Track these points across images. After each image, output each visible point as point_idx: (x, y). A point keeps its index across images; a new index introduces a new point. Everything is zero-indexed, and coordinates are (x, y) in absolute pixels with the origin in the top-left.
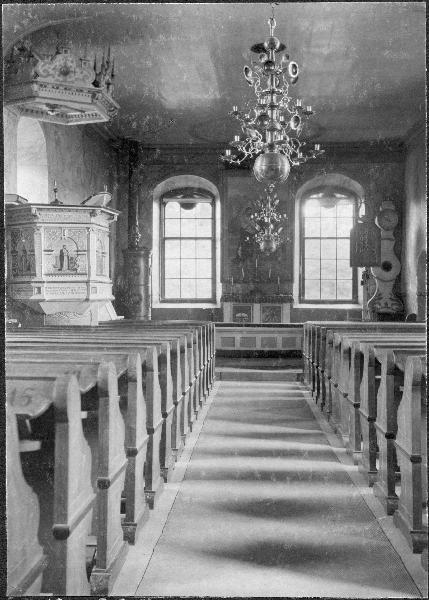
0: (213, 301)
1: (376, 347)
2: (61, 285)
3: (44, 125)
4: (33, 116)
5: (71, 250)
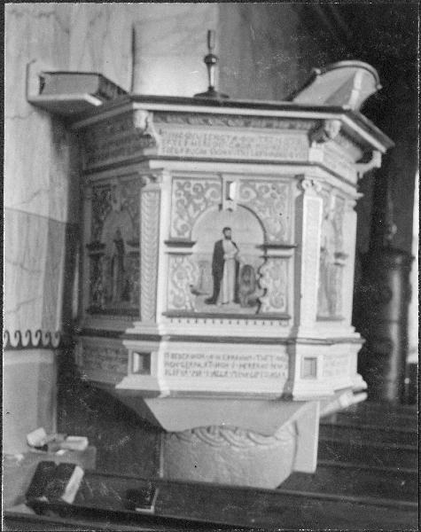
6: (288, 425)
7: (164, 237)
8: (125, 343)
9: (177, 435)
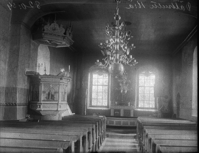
0: (108, 107)
1: (161, 146)
2: (51, 105)
3: (49, 47)
4: (44, 44)
5: (53, 92)
6: (58, 114)
7: (42, 91)
8: (37, 104)
9: (44, 116)
